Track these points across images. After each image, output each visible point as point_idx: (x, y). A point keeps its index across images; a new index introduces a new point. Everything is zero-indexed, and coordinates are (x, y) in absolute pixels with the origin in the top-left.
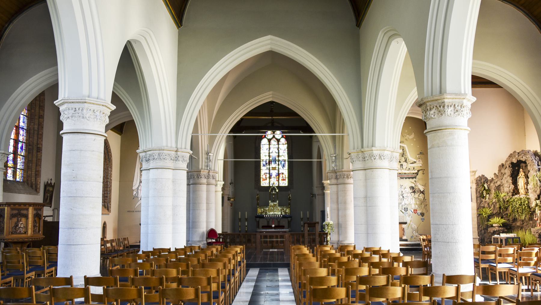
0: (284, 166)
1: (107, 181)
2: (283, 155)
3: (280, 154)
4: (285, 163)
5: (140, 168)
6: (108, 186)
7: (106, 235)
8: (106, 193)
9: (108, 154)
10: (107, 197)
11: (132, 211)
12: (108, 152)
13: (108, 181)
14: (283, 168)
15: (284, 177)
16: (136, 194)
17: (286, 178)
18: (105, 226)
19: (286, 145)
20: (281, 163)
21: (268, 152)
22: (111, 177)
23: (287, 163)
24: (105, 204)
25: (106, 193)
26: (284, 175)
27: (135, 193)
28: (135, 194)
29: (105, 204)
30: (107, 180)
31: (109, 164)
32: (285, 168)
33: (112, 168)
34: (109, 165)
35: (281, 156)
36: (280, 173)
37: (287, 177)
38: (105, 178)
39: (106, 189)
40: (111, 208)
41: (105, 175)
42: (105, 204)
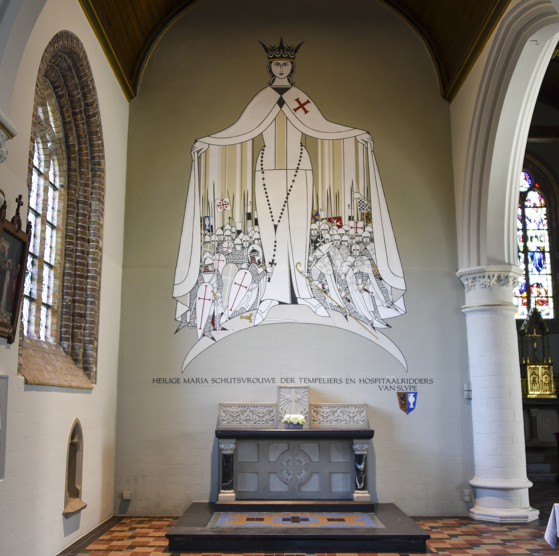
0: (540, 265)
1: (82, 252)
2: (536, 237)
3: (529, 234)
4: (544, 258)
5: (202, 220)
6: (88, 271)
7: (80, 483)
8: (79, 302)
9: (91, 140)
10: (83, 316)
11: (171, 381)
12: (91, 133)
13: (88, 253)
14: (539, 270)
15: (543, 294)
16: (189, 314)
17: (547, 297)
18: (76, 440)
19: (544, 209)
20: (532, 258)
21: (540, 209)
22: (100, 237)
23: (548, 255)
24: (73, 348)
25: (79, 302)
26: (542, 291)
27: (181, 309)
28: (184, 315)
29: (73, 348)
30: (82, 246)
31: (93, 183)
32: (543, 271)
33: (103, 203)
34: (93, 188)
35: (531, 238)
36: (531, 283)
37: (550, 294)
38: (77, 239)
39: (81, 283)
40: (96, 364)
41: (77, 227)
42: (77, 345)
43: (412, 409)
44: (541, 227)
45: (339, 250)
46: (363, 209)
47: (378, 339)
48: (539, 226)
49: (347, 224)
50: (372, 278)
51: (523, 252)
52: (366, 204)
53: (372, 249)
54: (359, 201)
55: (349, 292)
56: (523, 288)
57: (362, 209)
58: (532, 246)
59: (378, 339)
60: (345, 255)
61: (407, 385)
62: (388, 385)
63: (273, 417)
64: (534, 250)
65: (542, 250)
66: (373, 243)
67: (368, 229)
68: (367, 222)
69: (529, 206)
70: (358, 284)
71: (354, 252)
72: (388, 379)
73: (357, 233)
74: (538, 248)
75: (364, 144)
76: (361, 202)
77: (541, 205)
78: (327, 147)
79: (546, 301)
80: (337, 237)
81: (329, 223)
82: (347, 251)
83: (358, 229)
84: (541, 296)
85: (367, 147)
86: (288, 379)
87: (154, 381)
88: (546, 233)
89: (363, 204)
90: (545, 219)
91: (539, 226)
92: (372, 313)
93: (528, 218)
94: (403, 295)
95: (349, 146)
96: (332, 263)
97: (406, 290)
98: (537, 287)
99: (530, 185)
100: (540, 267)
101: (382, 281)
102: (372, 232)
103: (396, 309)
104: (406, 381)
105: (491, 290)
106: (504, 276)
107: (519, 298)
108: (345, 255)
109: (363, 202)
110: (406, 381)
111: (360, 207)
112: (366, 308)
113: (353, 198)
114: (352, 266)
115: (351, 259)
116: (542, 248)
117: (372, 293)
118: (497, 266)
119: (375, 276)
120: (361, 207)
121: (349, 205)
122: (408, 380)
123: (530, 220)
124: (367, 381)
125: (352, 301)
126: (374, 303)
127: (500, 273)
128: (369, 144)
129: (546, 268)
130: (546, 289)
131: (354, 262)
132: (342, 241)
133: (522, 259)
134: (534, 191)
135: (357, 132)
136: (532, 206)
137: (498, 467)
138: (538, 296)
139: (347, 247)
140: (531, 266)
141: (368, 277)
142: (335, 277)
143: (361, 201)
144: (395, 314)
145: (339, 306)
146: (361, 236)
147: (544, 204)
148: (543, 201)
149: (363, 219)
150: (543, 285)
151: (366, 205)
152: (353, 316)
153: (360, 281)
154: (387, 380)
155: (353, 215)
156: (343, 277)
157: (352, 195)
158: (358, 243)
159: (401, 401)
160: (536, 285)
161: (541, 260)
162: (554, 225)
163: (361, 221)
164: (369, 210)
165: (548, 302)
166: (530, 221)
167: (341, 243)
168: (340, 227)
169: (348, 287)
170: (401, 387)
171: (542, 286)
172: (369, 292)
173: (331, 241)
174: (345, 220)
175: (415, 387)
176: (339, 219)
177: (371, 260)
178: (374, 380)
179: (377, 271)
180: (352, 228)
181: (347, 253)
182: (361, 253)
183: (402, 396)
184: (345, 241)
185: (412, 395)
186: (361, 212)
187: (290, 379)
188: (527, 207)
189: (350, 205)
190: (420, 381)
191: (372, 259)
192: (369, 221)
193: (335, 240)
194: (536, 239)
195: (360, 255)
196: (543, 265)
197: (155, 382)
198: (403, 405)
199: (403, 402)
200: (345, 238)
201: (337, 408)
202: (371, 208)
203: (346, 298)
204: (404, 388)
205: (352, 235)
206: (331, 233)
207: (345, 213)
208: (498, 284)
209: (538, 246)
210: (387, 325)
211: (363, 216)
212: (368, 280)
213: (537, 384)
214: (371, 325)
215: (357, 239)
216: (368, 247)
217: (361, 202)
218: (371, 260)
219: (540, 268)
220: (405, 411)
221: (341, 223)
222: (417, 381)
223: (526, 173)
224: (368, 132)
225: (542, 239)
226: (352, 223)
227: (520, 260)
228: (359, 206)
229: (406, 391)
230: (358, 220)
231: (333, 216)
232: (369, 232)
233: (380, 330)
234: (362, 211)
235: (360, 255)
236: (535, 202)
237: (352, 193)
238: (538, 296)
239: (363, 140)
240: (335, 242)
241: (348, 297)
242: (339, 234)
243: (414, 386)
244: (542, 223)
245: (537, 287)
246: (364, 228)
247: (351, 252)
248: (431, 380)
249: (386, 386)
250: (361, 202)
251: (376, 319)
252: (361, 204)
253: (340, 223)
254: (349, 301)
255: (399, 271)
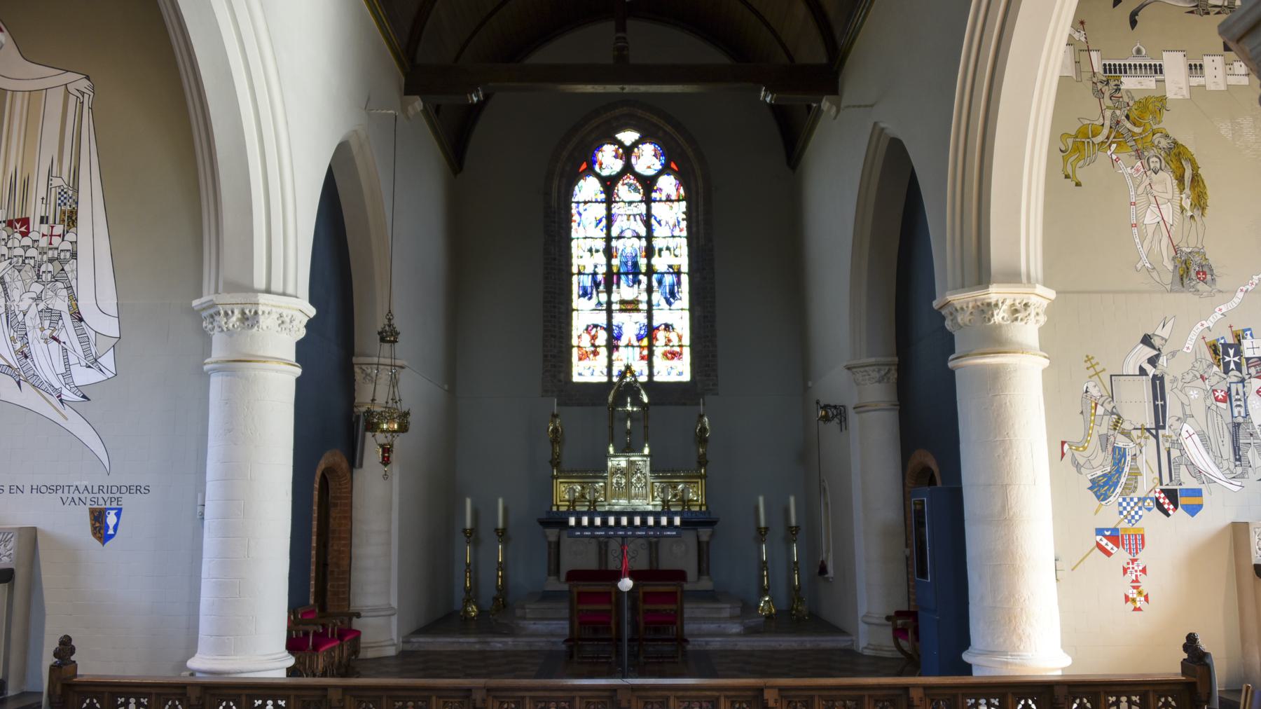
0: (672, 295)
2: (668, 249)
3: (657, 243)
4: (679, 283)
14: (669, 303)
15: (675, 341)
19: (683, 204)
20: (660, 282)
21: (676, 203)
23: (685, 279)
26: (673, 336)
35: (660, 250)
36: (655, 324)
37: (686, 341)
43: (111, 536)
44: (677, 232)
45: (19, 272)
46: (65, 204)
47: (67, 419)
48: (672, 230)
49: (37, 228)
50: (67, 317)
51: (645, 274)
52: (70, 195)
53: (72, 271)
54: (60, 191)
55: (28, 343)
56: (642, 332)
57: (62, 204)
58: (660, 263)
59: (67, 419)
60: (28, 281)
61: (106, 496)
62: (76, 495)
63: (11, 550)
64: (663, 271)
65: (676, 270)
66: (75, 261)
67: (70, 237)
68: (68, 225)
69: (658, 199)
70: (42, 329)
71: (44, 275)
72: (77, 487)
73: (51, 244)
74: (670, 266)
75: (77, 97)
76: (62, 193)
77: (679, 197)
78: (20, 103)
79: (678, 353)
80: (19, 251)
81: (9, 229)
82: (32, 274)
83: (53, 237)
84: (671, 344)
85: (83, 102)
86: (131, 488)
87: (32, 489)
88: (685, 241)
89: (65, 196)
90: (683, 220)
91: (672, 230)
92: (60, 376)
93: (655, 218)
94: (114, 346)
95: (54, 102)
96: (6, 294)
97: (120, 338)
98: (665, 330)
99: (662, 164)
100: (671, 297)
101: (83, 323)
102: (76, 242)
103: (101, 370)
104: (105, 490)
105: (231, 336)
106: (250, 311)
107: (636, 348)
108: (28, 281)
109: (65, 193)
110: (105, 490)
111: (60, 201)
112: (52, 367)
113: (50, 187)
114: (38, 299)
115: (37, 288)
116: (676, 267)
117: (64, 343)
118: (232, 294)
119: (71, 315)
120: (62, 201)
121: (43, 199)
122: (110, 488)
123: (660, 221)
124: (43, 489)
125: (30, 357)
126: (66, 360)
127: (242, 306)
128: (86, 96)
129: (681, 299)
130: (680, 333)
131: (42, 292)
132: (26, 258)
133: (644, 286)
134: (668, 174)
135: (71, 77)
136: (664, 198)
137: (211, 636)
138: (666, 345)
139: (34, 267)
140: (657, 297)
141: (61, 316)
142: (7, 317)
143: (62, 190)
144: (100, 377)
145: (9, 366)
146: (57, 249)
147: (683, 194)
148: (682, 191)
149: (64, 221)
150: (674, 326)
151: (70, 198)
152: (31, 381)
153: (47, 323)
154: (74, 487)
155: (47, 215)
156: (20, 317)
157: (50, 182)
158: (51, 261)
159: (94, 522)
160: (663, 327)
161: (673, 285)
162: (694, 229)
163: (60, 224)
164: (74, 206)
165: (681, 354)
166: (659, 223)
167: (23, 262)
168: (24, 234)
169: (26, 334)
170: (96, 500)
171: (673, 329)
172: (59, 342)
173: (9, 258)
174: (35, 224)
175: (120, 499)
176: (25, 221)
177: (69, 288)
178: (54, 488)
179: (75, 307)
180: (43, 235)
181: (32, 278)
182: (54, 278)
183: (96, 515)
184: (31, 258)
185: (113, 513)
186: (61, 209)
187: (135, 488)
188: (655, 201)
189: (45, 197)
190: (129, 489)
191: (71, 286)
192: (73, 224)
193: (15, 256)
194: (668, 251)
195: (53, 280)
196: (677, 295)
197: (34, 491)
198: (98, 529)
199: (97, 525)
200: (32, 252)
201: (11, 535)
202: (77, 203)
203: (22, 352)
204: (101, 501)
205: (43, 248)
206: (10, 245)
207: (35, 211)
208: (242, 325)
209: (670, 263)
210: (84, 397)
211: (63, 217)
212: (60, 322)
213: (622, 488)
214: (58, 397)
215: (50, 254)
216: (67, 268)
217: (62, 193)
218: (69, 288)
219: (672, 300)
220: (99, 539)
221: (28, 228)
222: (124, 490)
223: (657, 146)
224: (88, 76)
225: (676, 253)
226: (45, 229)
227: (641, 286)
228: (60, 199)
229: (103, 506)
230: (55, 223)
231: (16, 217)
232: (71, 242)
233: (71, 404)
234: (63, 208)
235: (53, 280)
236: (669, 193)
237: (50, 178)
238: (666, 345)
239: (78, 90)
240: (15, 259)
241: (26, 350)
242: (23, 247)
243: (118, 498)
244: (679, 226)
245: (665, 330)
246: (63, 236)
247: (39, 276)
248: (147, 488)
249: (73, 498)
250: (62, 193)
251: (67, 386)
252: (62, 196)
253: (25, 229)
254: (26, 357)
255: (110, 304)
